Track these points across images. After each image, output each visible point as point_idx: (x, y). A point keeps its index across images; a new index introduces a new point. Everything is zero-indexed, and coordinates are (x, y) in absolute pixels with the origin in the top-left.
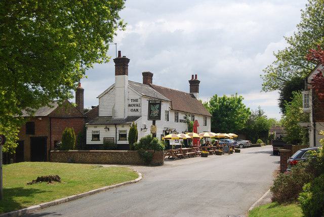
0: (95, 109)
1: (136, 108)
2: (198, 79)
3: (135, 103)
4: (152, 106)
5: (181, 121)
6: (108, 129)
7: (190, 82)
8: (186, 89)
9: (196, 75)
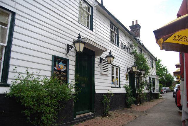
9: (136, 21)
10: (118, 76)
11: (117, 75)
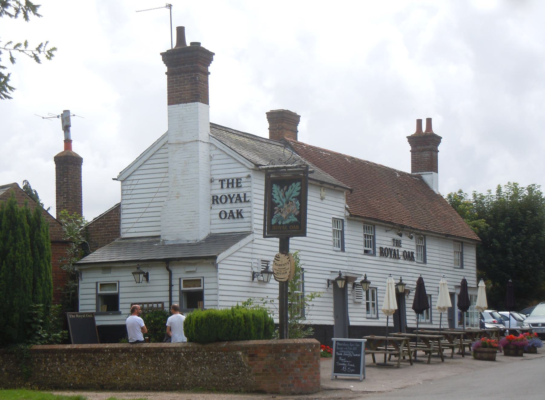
0: (111, 219)
1: (235, 207)
2: (436, 130)
3: (232, 191)
4: (275, 188)
5: (384, 252)
6: (147, 276)
7: (412, 140)
8: (401, 161)
9: (429, 121)
10: (375, 302)
11: (373, 300)
